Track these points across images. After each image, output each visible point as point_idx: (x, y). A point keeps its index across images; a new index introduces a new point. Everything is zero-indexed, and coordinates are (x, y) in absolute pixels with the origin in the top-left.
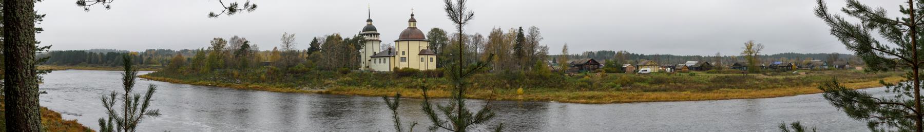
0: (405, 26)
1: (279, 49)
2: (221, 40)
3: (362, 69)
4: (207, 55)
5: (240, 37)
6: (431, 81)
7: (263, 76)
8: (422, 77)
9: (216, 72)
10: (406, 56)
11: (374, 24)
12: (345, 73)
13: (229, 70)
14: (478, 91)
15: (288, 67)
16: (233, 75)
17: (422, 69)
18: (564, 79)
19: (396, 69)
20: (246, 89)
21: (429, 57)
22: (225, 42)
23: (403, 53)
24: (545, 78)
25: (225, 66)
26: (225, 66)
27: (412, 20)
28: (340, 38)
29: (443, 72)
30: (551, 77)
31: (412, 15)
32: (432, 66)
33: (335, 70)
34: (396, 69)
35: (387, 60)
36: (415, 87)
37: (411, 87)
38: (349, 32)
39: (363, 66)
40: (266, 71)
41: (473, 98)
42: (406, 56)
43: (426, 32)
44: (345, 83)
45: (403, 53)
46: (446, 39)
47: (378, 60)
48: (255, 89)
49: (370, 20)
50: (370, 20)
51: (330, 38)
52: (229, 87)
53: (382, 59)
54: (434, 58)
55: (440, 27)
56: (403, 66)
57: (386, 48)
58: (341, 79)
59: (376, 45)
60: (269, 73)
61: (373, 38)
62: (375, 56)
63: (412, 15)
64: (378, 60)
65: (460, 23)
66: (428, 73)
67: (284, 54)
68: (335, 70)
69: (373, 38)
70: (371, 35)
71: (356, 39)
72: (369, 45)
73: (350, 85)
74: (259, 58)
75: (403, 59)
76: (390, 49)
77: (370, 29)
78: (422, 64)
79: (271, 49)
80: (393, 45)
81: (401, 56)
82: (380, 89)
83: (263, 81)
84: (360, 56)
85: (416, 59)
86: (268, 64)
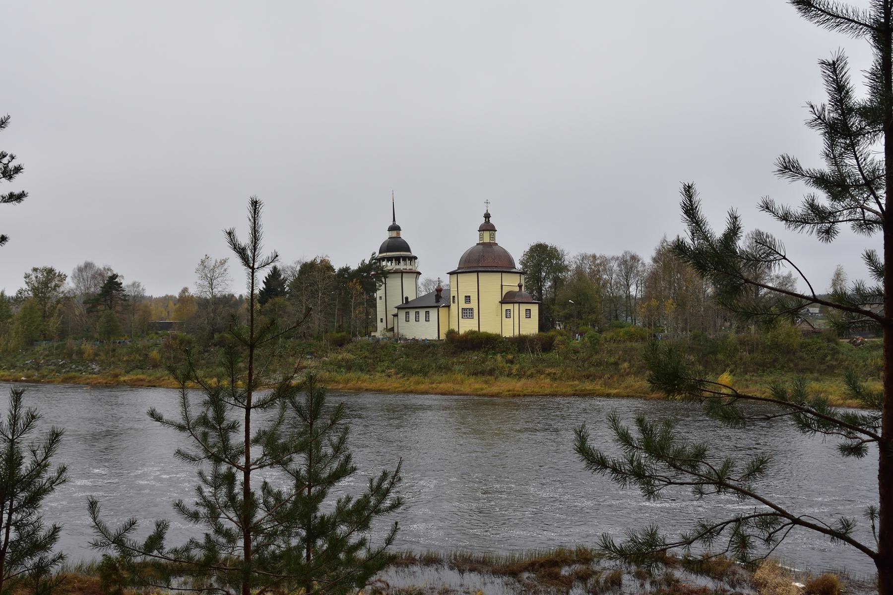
0: (472, 239)
1: (193, 291)
2: (50, 271)
3: (378, 334)
4: (15, 310)
5: (100, 265)
6: (527, 358)
7: (154, 354)
8: (505, 351)
9: (41, 347)
10: (473, 304)
11: (404, 235)
12: (340, 343)
13: (70, 343)
14: (630, 380)
15: (213, 332)
16: (80, 353)
17: (508, 333)
18: (835, 352)
19: (451, 334)
20: (114, 384)
21: (523, 307)
22: (62, 278)
23: (468, 299)
24: (788, 351)
25: (63, 333)
26: (63, 333)
27: (488, 227)
28: (330, 268)
29: (552, 339)
30: (802, 346)
31: (487, 216)
32: (530, 327)
33: (319, 338)
34: (451, 334)
35: (433, 313)
36: (491, 372)
37: (483, 373)
38: (350, 254)
39: (381, 326)
40: (162, 342)
41: (618, 396)
42: (473, 304)
43: (517, 253)
44: (339, 365)
45: (468, 299)
46: (563, 268)
47: (412, 314)
48: (135, 385)
49: (395, 228)
50: (395, 228)
51: (308, 269)
52: (71, 381)
53: (422, 313)
54: (535, 309)
55: (550, 242)
56: (466, 326)
57: (432, 288)
58: (331, 356)
59: (408, 281)
60: (168, 346)
61: (402, 266)
62: (407, 306)
63: (487, 216)
64: (412, 314)
65: (253, 268)
66: (521, 343)
67: (203, 303)
68: (319, 338)
69: (402, 266)
70: (398, 259)
71: (364, 269)
72: (393, 283)
73: (349, 369)
74: (147, 313)
75: (467, 313)
76: (439, 290)
77: (396, 247)
78: (508, 322)
79: (176, 294)
80: (446, 280)
81: (463, 305)
82: (414, 378)
83: (155, 366)
84: (374, 306)
85: (494, 312)
86: (168, 326)
